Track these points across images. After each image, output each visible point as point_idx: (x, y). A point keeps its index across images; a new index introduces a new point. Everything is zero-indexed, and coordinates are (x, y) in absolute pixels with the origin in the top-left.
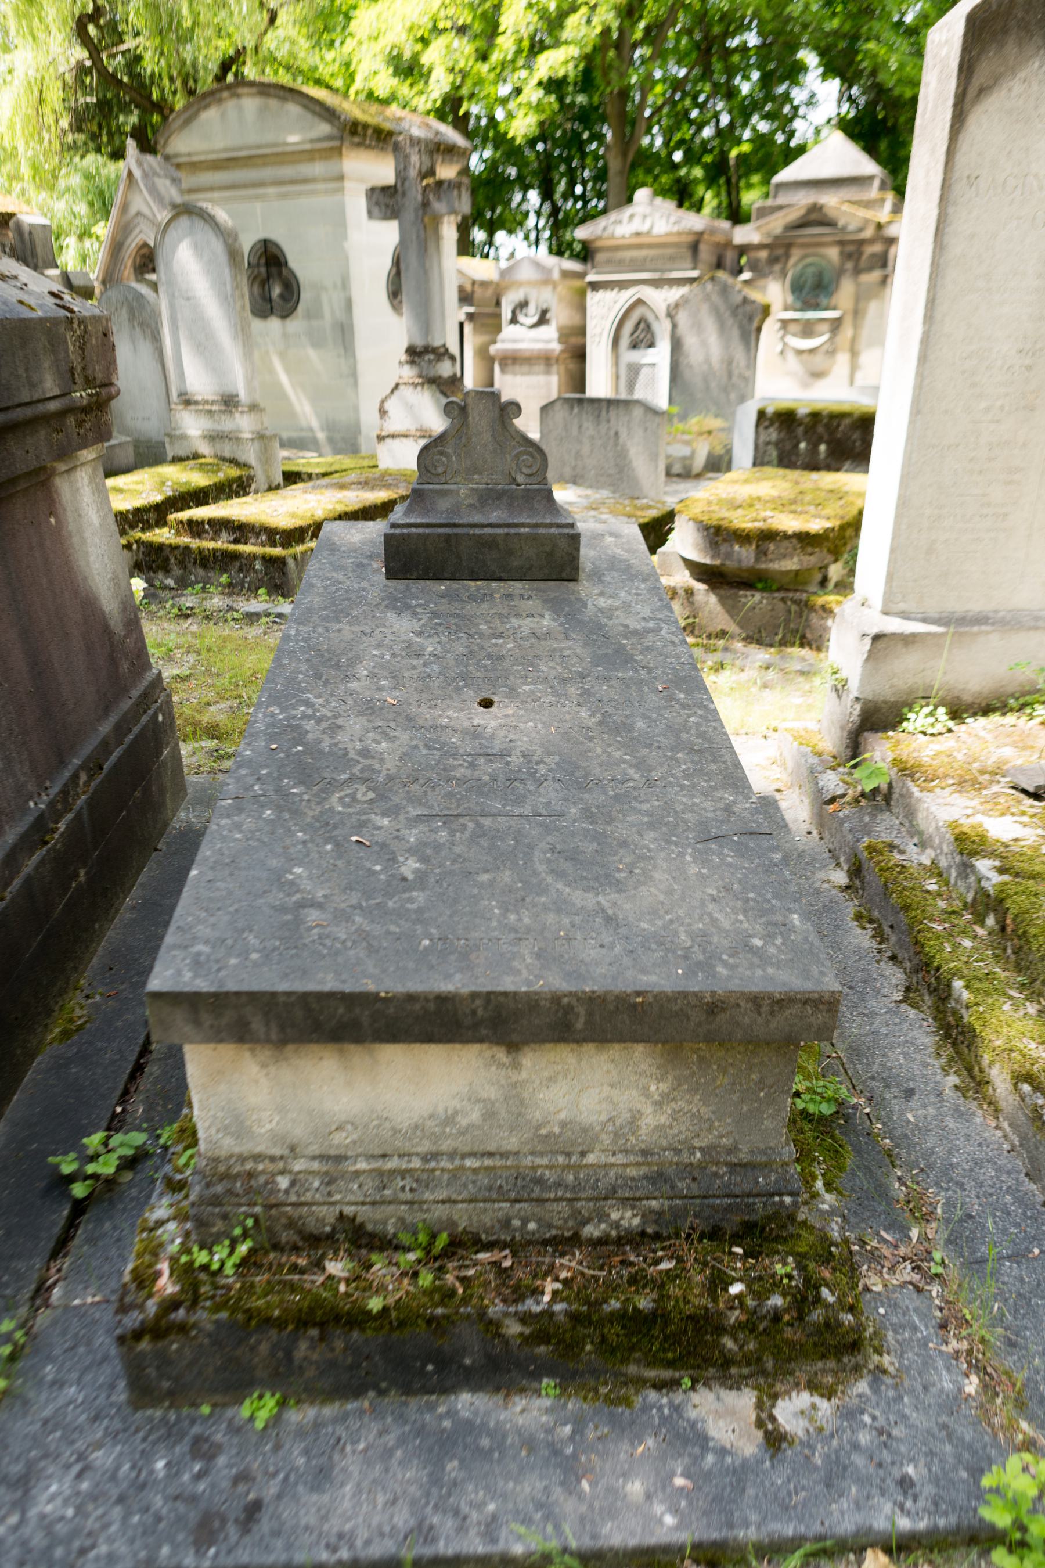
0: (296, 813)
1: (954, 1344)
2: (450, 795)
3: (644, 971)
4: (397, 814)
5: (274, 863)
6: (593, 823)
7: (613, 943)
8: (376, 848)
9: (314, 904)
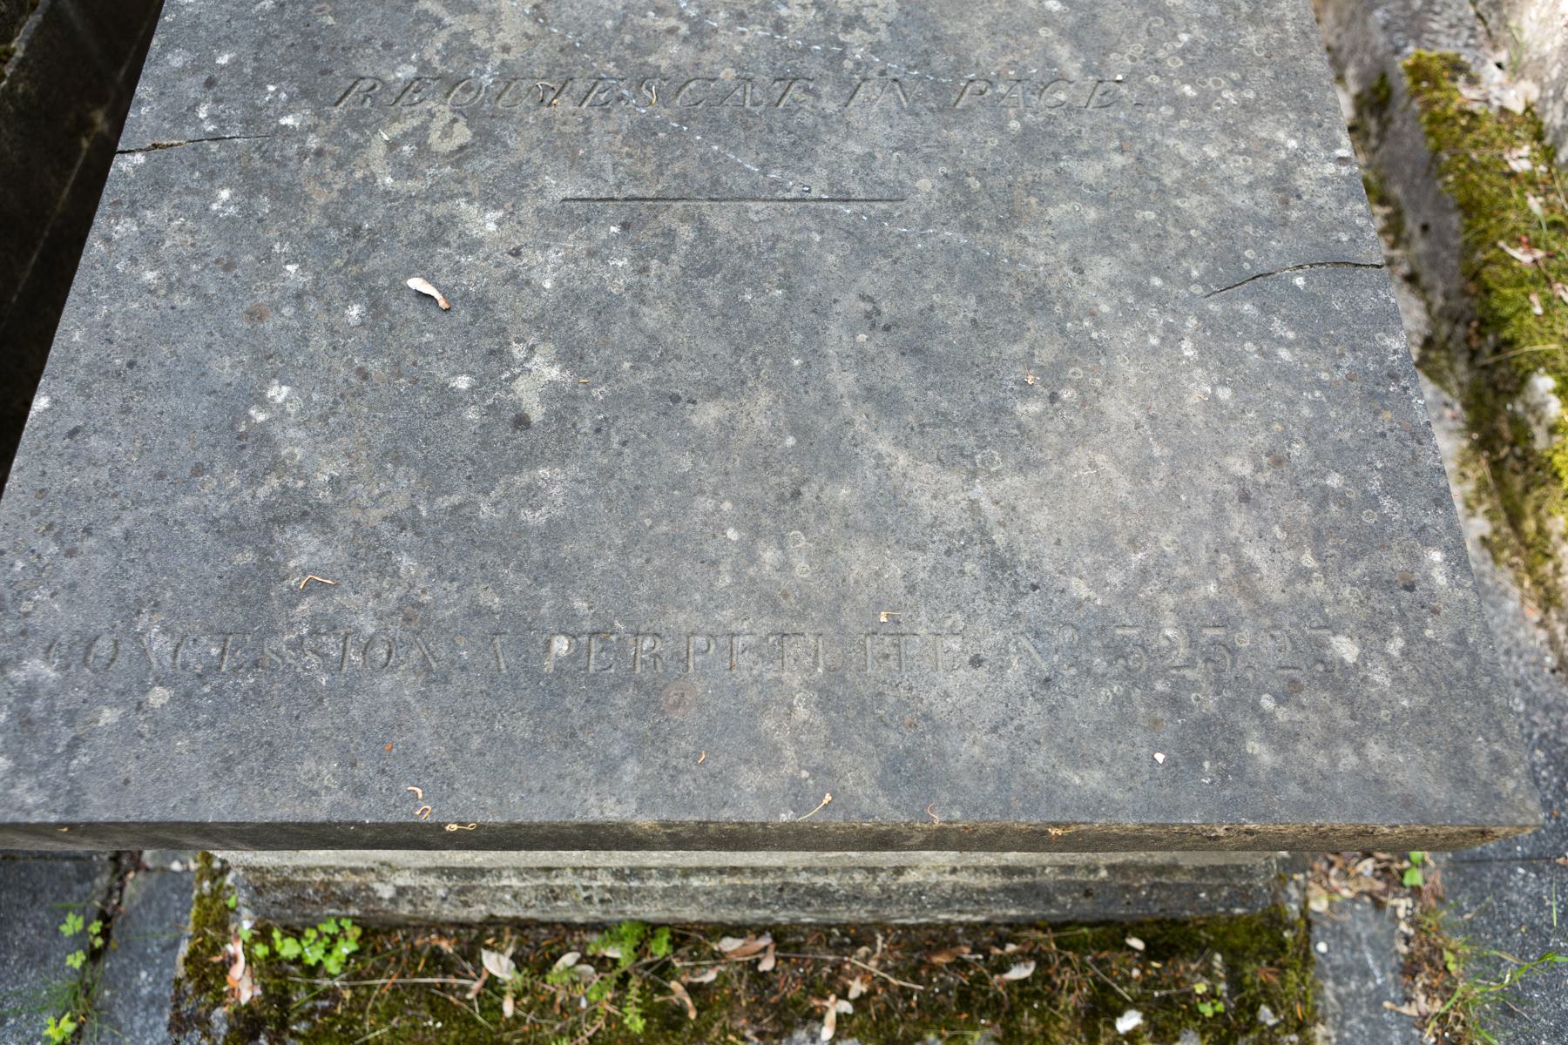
0: (289, 196)
1: (1422, 1004)
2: (644, 130)
3: (1077, 759)
4: (517, 196)
5: (224, 369)
6: (971, 226)
7: (1002, 651)
8: (463, 315)
9: (315, 516)
